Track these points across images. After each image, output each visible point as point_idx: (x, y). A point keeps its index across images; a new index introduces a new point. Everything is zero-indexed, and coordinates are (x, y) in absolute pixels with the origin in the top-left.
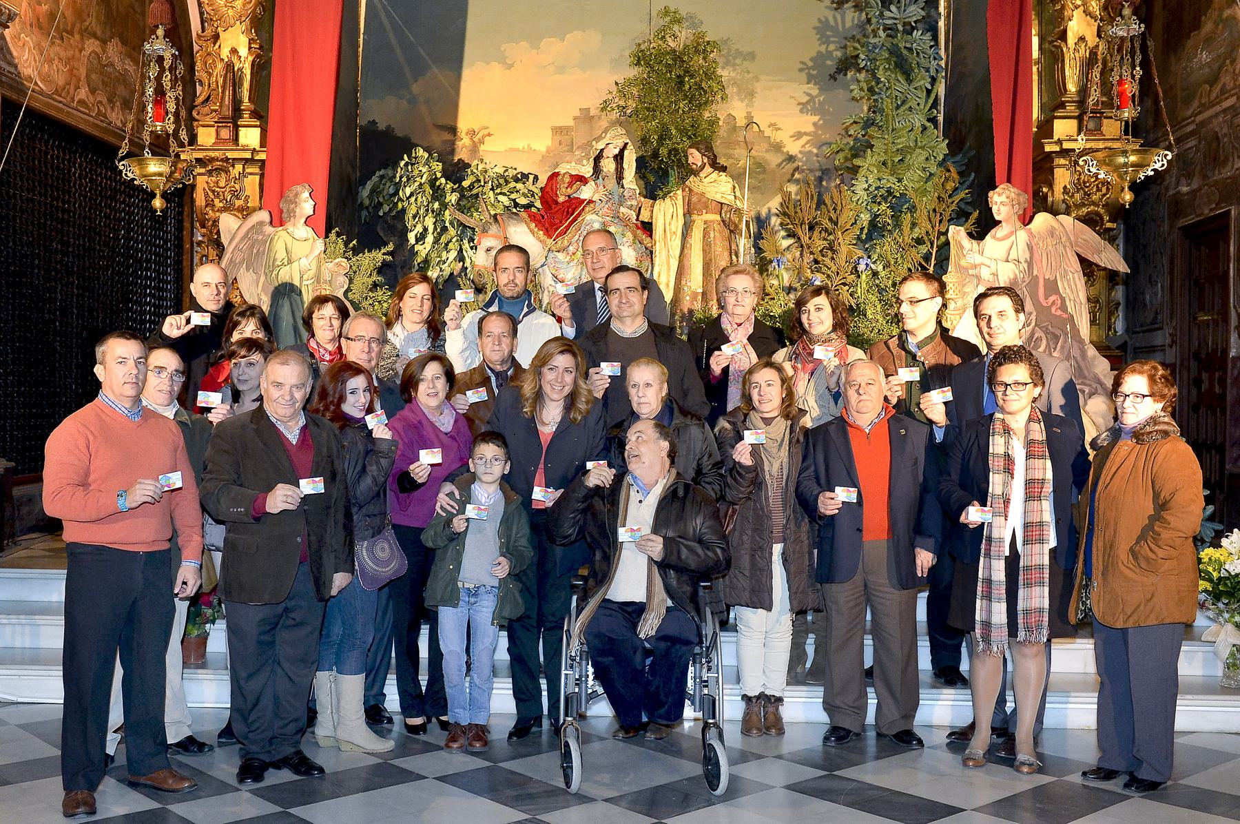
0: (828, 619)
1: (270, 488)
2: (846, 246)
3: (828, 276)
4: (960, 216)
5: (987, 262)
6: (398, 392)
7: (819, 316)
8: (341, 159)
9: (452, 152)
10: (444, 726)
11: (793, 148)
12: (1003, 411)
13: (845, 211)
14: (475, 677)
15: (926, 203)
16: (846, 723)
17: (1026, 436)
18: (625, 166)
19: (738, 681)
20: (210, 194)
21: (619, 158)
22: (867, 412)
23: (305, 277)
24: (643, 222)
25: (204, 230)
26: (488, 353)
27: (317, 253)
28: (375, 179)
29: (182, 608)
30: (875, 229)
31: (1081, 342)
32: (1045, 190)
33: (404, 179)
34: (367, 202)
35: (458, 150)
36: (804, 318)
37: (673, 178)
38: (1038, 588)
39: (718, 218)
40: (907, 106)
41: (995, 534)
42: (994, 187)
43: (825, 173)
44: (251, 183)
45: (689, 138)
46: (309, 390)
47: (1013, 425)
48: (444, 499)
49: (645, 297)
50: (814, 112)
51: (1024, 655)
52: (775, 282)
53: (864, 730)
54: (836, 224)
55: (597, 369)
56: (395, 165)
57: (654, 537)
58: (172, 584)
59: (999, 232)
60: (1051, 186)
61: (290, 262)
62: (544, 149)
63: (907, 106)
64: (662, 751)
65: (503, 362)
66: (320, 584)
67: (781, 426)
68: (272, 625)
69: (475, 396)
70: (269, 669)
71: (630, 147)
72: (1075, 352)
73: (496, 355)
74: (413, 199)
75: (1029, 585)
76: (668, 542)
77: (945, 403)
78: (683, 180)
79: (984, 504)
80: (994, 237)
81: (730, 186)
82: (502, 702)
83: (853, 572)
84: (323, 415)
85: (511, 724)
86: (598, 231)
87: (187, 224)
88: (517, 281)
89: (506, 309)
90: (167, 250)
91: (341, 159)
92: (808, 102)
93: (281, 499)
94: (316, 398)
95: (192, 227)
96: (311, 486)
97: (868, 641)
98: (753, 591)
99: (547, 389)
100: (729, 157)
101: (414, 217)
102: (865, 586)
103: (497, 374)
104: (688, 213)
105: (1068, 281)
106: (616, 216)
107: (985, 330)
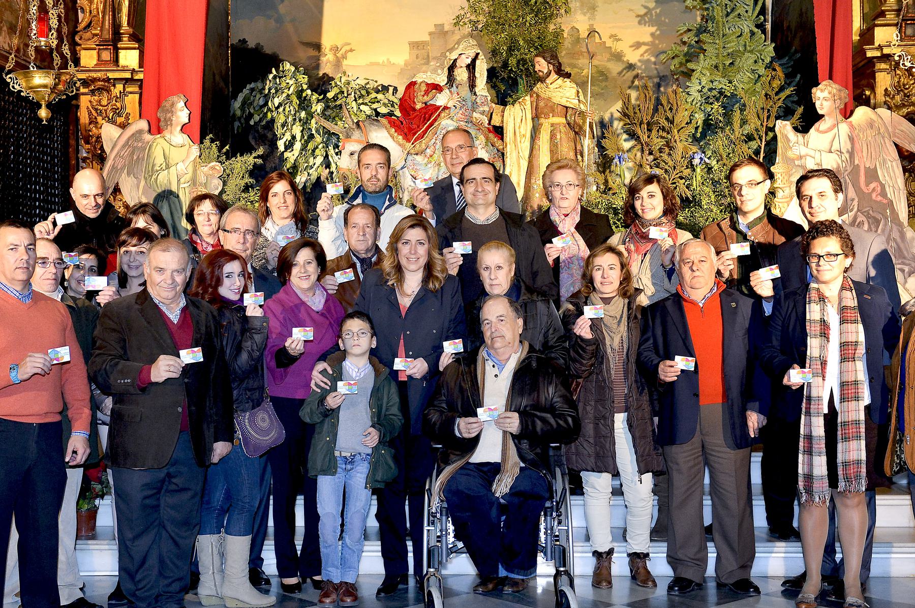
0: (669, 482)
1: (153, 360)
2: (682, 143)
3: (666, 171)
4: (786, 113)
5: (812, 153)
6: (273, 276)
7: (651, 203)
8: (214, 75)
9: (317, 67)
10: (317, 585)
11: (633, 57)
12: (818, 281)
13: (680, 109)
14: (347, 540)
15: (755, 103)
16: (689, 574)
17: (840, 303)
18: (477, 75)
19: (588, 538)
20: (94, 112)
21: (471, 67)
22: (700, 287)
23: (182, 180)
24: (494, 126)
25: (88, 146)
26: (353, 242)
27: (192, 158)
28: (246, 91)
29: (74, 479)
30: (709, 126)
31: (900, 224)
32: (868, 93)
33: (273, 91)
34: (239, 113)
35: (322, 65)
36: (638, 204)
37: (522, 83)
38: (855, 442)
39: (564, 120)
40: (736, 13)
41: (814, 394)
42: (817, 84)
43: (662, 80)
44: (132, 101)
45: (537, 48)
46: (188, 274)
47: (827, 294)
48: (318, 376)
49: (497, 188)
50: (652, 23)
51: (846, 506)
52: (618, 179)
53: (705, 581)
54: (672, 122)
55: (450, 249)
56: (264, 78)
57: (510, 414)
58: (62, 452)
59: (822, 125)
60: (873, 88)
61: (168, 167)
62: (402, 63)
63: (736, 13)
64: (518, 602)
65: (367, 251)
66: (202, 452)
67: (620, 304)
68: (158, 488)
69: (343, 277)
70: (156, 530)
71: (481, 57)
72: (895, 234)
73: (361, 246)
74: (281, 109)
75: (846, 439)
76: (523, 414)
77: (772, 280)
78: (530, 87)
79: (803, 366)
80: (818, 130)
81: (574, 91)
82: (371, 564)
83: (692, 433)
84: (203, 298)
85: (379, 582)
86: (453, 131)
87: (72, 142)
88: (379, 176)
89: (368, 201)
90: (54, 165)
91: (214, 75)
92: (646, 14)
93: (164, 369)
94: (195, 282)
95: (78, 145)
96: (191, 356)
97: (707, 502)
98: (597, 455)
99: (403, 262)
100: (574, 66)
101: (283, 126)
102: (703, 447)
103: (362, 261)
104: (536, 117)
105: (887, 169)
106: (469, 121)
107: (807, 209)
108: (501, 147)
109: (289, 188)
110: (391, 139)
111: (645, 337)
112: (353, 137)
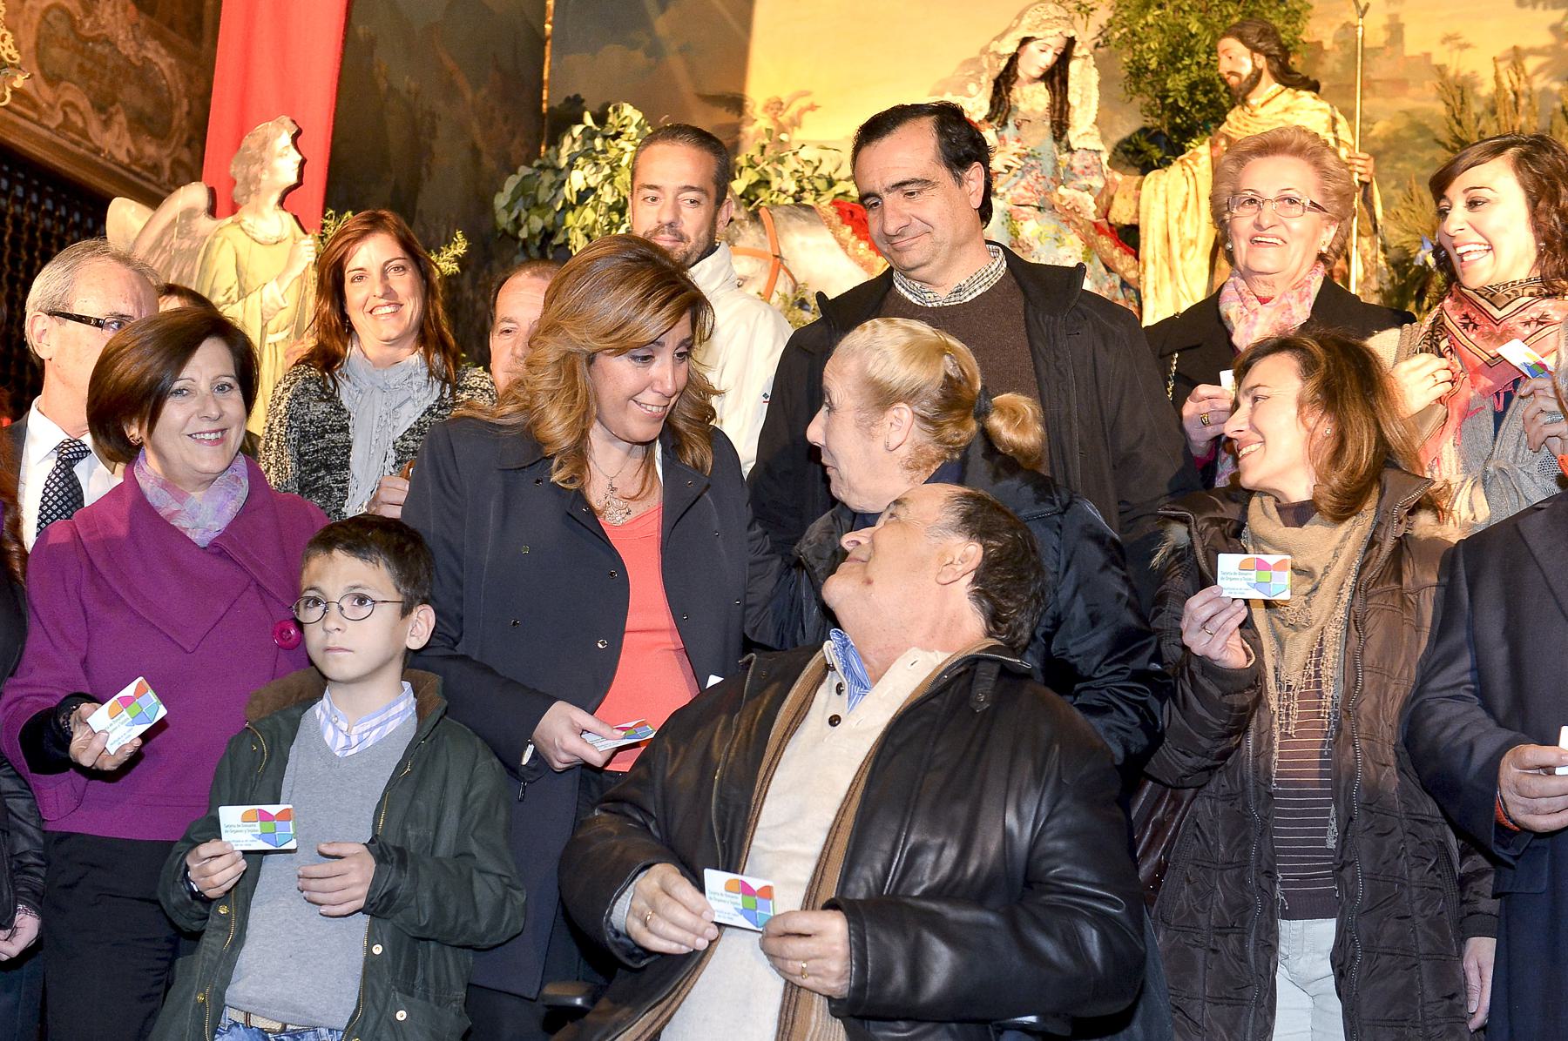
18: (1073, 98)
21: (1056, 77)
23: (271, 326)
27: (298, 269)
61: (243, 294)
81: (1326, 117)
108: (1131, 275)
109: (397, 251)
110: (840, 252)
111: (1443, 648)
112: (739, 244)
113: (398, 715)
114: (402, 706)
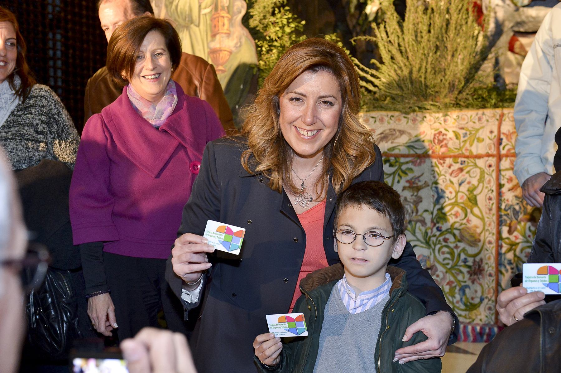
23: (203, 5)
113: (383, 292)
114: (386, 287)
